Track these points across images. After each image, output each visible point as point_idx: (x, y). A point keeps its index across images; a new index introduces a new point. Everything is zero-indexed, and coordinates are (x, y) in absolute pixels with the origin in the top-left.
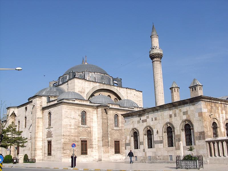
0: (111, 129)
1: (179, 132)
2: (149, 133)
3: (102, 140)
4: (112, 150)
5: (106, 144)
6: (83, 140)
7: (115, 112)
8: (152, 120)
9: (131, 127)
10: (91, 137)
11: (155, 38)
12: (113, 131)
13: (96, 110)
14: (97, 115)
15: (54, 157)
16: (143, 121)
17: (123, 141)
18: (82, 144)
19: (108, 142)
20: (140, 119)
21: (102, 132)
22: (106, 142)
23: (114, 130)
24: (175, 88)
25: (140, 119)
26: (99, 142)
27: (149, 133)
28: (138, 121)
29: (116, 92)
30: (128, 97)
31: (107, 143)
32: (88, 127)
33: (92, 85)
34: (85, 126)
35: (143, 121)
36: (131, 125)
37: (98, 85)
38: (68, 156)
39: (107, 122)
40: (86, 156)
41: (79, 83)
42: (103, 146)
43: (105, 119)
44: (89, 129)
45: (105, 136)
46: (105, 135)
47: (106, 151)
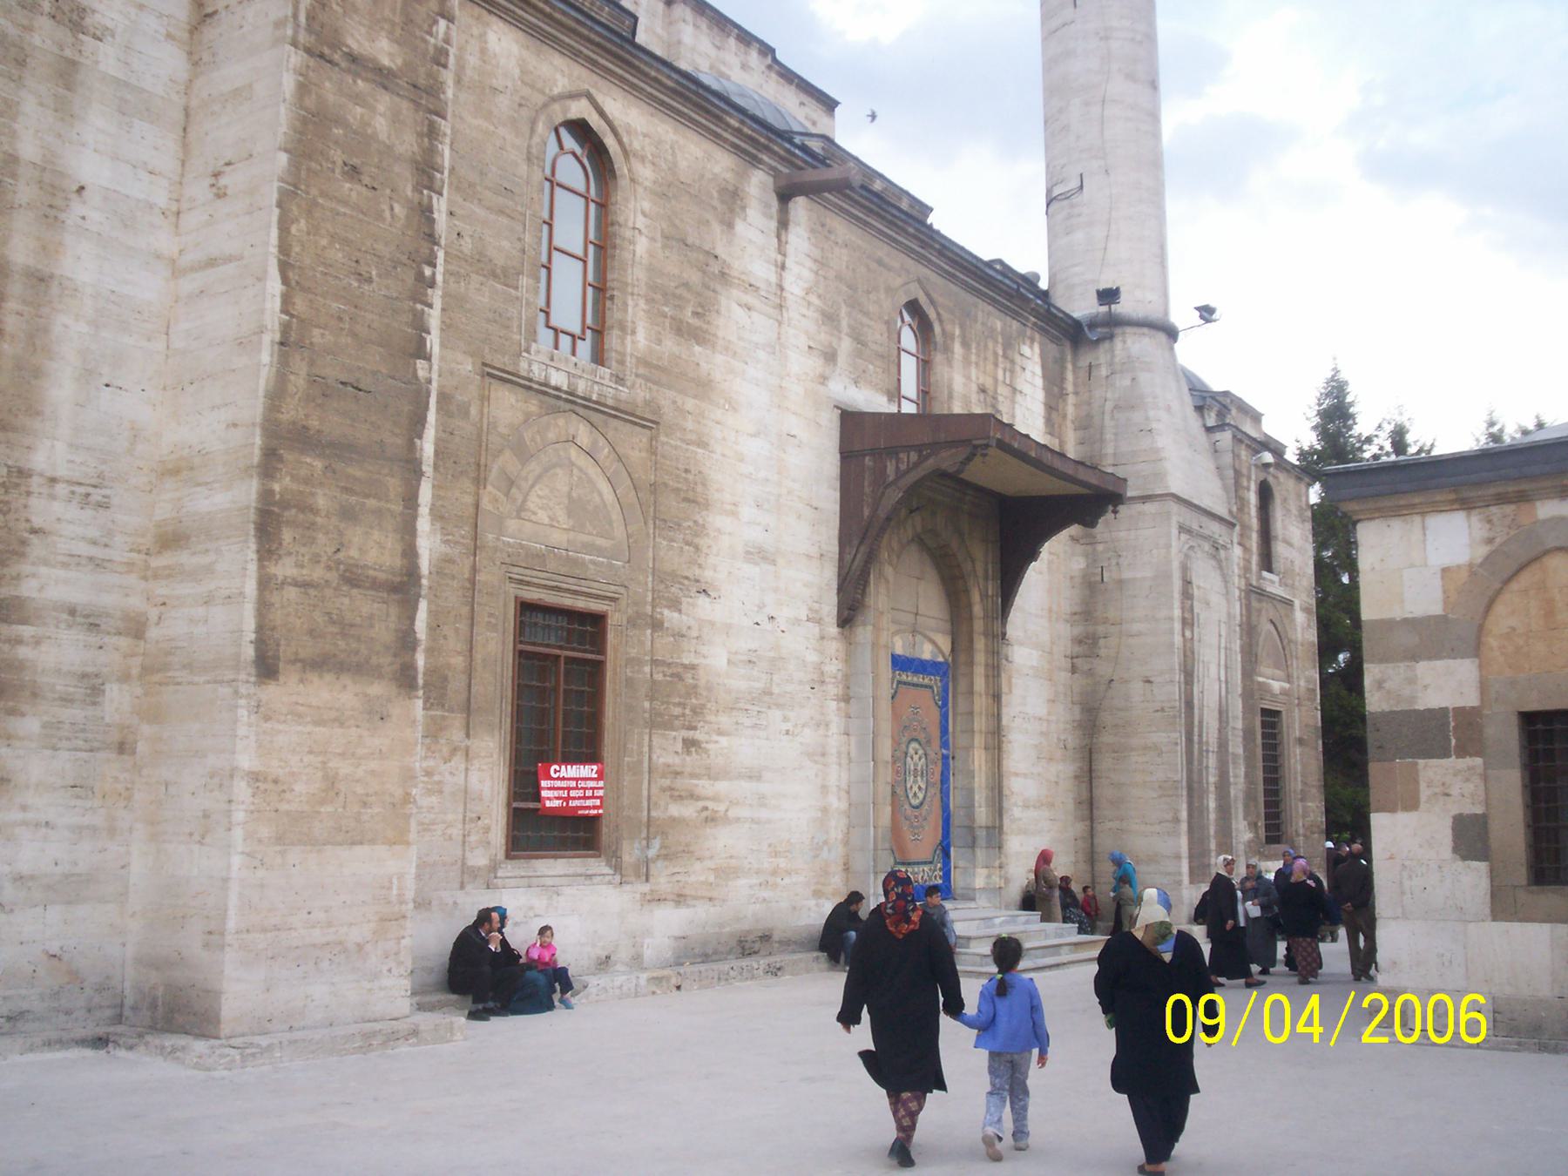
0: (467, 366)
4: (452, 773)
5: (345, 628)
7: (561, 85)
12: (507, 406)
17: (657, 625)
19: (404, 587)
22: (353, 578)
26: (184, 558)
31: (363, 605)
42: (266, 668)
43: (383, 77)
45: (338, 450)
46: (341, 421)
47: (331, 782)
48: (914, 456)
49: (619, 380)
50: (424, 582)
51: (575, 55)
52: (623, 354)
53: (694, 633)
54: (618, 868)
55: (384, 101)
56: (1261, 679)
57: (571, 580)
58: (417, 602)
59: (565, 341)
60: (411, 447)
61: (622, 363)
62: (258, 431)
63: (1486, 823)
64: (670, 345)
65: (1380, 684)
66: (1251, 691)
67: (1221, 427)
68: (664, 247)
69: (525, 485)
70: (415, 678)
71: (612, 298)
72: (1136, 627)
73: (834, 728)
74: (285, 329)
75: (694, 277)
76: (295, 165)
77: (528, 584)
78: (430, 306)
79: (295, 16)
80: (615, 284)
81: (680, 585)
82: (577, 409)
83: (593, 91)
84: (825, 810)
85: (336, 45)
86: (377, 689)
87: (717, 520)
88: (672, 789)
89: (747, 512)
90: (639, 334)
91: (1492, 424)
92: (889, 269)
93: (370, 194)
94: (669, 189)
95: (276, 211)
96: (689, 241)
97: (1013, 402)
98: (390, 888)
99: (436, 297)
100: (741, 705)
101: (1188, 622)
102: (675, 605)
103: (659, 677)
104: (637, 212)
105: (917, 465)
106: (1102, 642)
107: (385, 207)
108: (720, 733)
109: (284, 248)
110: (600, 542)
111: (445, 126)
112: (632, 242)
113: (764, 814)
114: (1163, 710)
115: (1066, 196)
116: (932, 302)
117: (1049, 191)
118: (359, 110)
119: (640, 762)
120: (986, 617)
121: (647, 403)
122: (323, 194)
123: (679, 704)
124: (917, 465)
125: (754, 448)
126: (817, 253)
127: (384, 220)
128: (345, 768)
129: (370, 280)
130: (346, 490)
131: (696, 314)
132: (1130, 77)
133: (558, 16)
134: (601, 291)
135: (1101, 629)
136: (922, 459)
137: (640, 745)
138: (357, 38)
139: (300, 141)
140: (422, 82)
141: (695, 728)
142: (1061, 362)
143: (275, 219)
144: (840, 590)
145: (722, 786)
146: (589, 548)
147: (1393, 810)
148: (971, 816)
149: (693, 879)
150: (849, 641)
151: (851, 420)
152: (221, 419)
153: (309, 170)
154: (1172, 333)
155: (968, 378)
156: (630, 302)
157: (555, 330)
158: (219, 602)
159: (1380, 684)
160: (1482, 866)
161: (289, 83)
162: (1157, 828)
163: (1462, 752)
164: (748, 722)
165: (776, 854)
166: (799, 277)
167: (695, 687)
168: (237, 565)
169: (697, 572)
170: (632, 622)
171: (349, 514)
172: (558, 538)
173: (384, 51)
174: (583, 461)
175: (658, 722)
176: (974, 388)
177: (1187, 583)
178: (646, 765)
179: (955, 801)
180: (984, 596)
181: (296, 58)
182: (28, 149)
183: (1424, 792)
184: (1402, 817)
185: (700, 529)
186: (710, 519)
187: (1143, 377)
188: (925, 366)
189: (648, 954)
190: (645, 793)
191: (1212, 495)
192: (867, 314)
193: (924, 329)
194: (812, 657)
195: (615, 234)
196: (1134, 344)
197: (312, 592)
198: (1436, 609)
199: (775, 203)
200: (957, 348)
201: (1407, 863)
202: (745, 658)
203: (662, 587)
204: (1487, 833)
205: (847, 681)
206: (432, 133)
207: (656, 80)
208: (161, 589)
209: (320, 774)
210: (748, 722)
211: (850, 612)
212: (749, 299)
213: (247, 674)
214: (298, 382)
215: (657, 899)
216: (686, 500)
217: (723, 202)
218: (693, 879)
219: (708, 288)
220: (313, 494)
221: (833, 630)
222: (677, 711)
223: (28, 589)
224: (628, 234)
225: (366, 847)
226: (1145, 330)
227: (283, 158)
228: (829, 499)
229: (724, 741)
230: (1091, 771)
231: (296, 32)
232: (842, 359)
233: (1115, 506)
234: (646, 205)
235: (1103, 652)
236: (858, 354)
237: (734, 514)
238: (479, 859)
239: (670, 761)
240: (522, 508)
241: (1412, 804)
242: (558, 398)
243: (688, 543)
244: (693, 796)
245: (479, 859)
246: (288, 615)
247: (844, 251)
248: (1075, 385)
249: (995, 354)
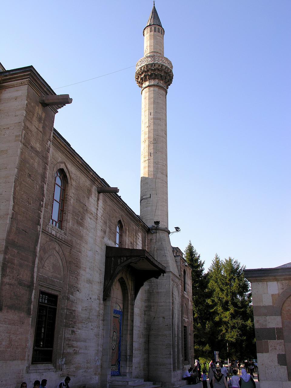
7: (60, 160)
17: (68, 299)
21: (10, 211)
22: (20, 283)
47: (11, 341)
48: (125, 259)
49: (65, 234)
50: (35, 285)
52: (67, 228)
53: (75, 302)
54: (55, 367)
55: (37, 159)
56: (184, 318)
57: (52, 286)
58: (33, 291)
59: (54, 223)
61: (66, 230)
62: (5, 241)
63: (285, 356)
64: (76, 226)
65: (258, 322)
66: (183, 321)
67: (178, 256)
68: (76, 202)
69: (45, 260)
70: (30, 312)
71: (65, 213)
72: (163, 304)
73: (101, 328)
74: (13, 214)
75: (81, 210)
76: (18, 172)
77: (43, 286)
78: (42, 212)
79: (22, 135)
80: (66, 210)
81: (74, 288)
82: (56, 240)
83: (66, 162)
84: (98, 351)
85: (29, 144)
86: (22, 315)
87: (82, 272)
88: (68, 344)
89: (88, 270)
90: (70, 224)
91: (217, 258)
92: (116, 212)
93: (32, 182)
94: (78, 188)
95: (14, 183)
96: (81, 201)
98: (20, 374)
99: (43, 209)
100: (83, 321)
101: (173, 304)
103: (68, 313)
104: (71, 192)
105: (126, 261)
106: (152, 308)
107: (35, 186)
108: (79, 329)
109: (14, 193)
110: (58, 276)
112: (70, 200)
114: (167, 325)
115: (146, 198)
116: (123, 221)
117: (141, 197)
118: (32, 160)
119: (62, 336)
120: (131, 300)
121: (71, 241)
122: (23, 181)
123: (71, 320)
124: (126, 261)
125: (90, 254)
126: (104, 207)
127: (34, 189)
129: (30, 204)
130: (21, 259)
131: (81, 219)
132: (162, 173)
133: (61, 143)
134: (62, 211)
135: (152, 304)
136: (127, 259)
137: (63, 332)
138: (33, 143)
139: (20, 166)
140: (44, 155)
141: (74, 327)
142: (145, 237)
143: (13, 185)
144: (104, 292)
145: (79, 343)
146: (56, 278)
147: (263, 353)
148: (126, 353)
149: (71, 370)
150: (105, 305)
151: (109, 249)
153: (21, 174)
154: (169, 233)
155: (129, 240)
156: (69, 215)
157: (53, 220)
159: (258, 322)
160: (286, 367)
161: (19, 151)
162: (165, 356)
163: (279, 338)
164: (84, 326)
166: (100, 212)
167: (75, 316)
169: (77, 285)
172: (50, 274)
173: (38, 146)
175: (67, 326)
176: (130, 242)
177: (173, 293)
178: (63, 337)
179: (123, 348)
181: (21, 145)
183: (270, 349)
184: (265, 354)
185: (78, 274)
186: (80, 271)
187: (163, 243)
188: (121, 236)
190: (63, 346)
191: (177, 274)
192: (112, 222)
193: (121, 227)
194: (98, 309)
195: (67, 198)
196: (161, 234)
197: (12, 287)
198: (271, 304)
199: (97, 194)
201: (266, 366)
202: (85, 308)
203: (70, 289)
204: (286, 358)
205: (105, 315)
207: (78, 161)
209: (8, 339)
210: (84, 326)
212: (91, 216)
214: (14, 229)
216: (76, 266)
217: (88, 192)
218: (71, 370)
219: (84, 213)
220: (14, 259)
221: (102, 302)
222: (71, 322)
224: (70, 198)
225: (16, 361)
226: (164, 232)
227: (16, 170)
229: (79, 331)
230: (149, 341)
231: (22, 139)
232: (107, 233)
233: (163, 274)
234: (74, 191)
235: (153, 310)
236: (110, 232)
237: (85, 270)
239: (68, 336)
240: (43, 266)
241: (267, 351)
242: (53, 237)
243: (76, 278)
244: (73, 347)
246: (6, 293)
247: (109, 207)
248: (148, 243)
249: (134, 234)
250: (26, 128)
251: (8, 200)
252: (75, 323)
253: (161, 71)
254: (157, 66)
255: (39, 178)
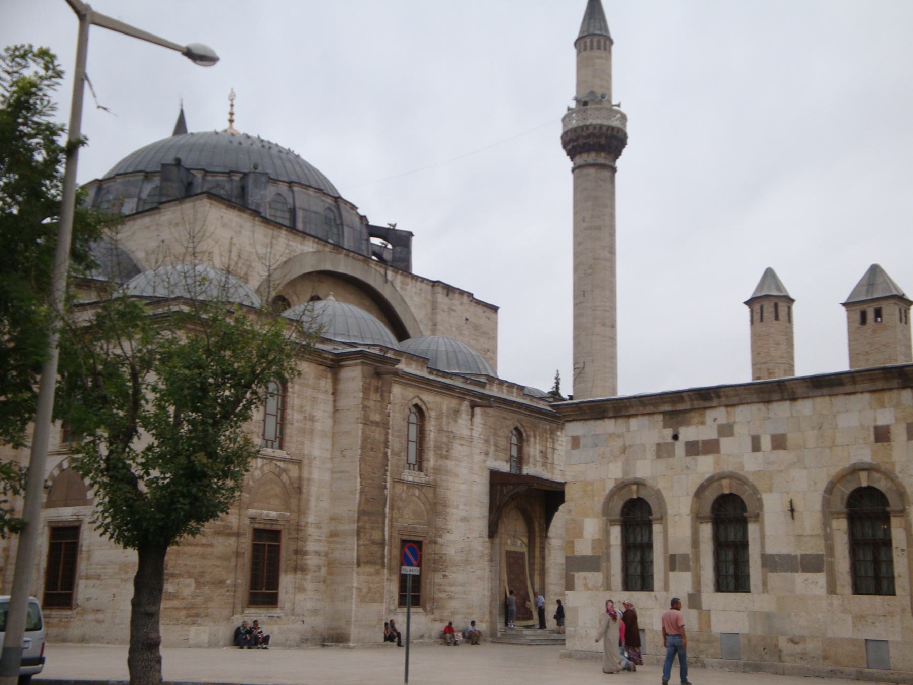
1: (679, 528)
2: (729, 513)
3: (358, 535)
6: (262, 526)
7: (411, 395)
8: (756, 446)
9: (615, 472)
10: (301, 511)
11: (599, 48)
13: (329, 375)
14: (335, 401)
15: (91, 617)
16: (693, 449)
17: (435, 543)
18: (256, 549)
19: (382, 544)
20: (675, 437)
21: (358, 487)
22: (373, 543)
23: (403, 482)
24: (775, 300)
25: (675, 437)
26: (338, 539)
27: (729, 513)
28: (659, 445)
29: (386, 292)
30: (439, 327)
31: (375, 548)
32: (292, 461)
33: (285, 246)
34: (280, 453)
35: (693, 449)
36: (611, 466)
37: (311, 250)
38: (184, 613)
39: (382, 439)
40: (276, 612)
41: (224, 225)
42: (358, 565)
43: (377, 424)
44: (294, 471)
46: (372, 508)
47: (369, 588)
51: (414, 386)
60: (384, 511)
81: (439, 531)
86: (378, 567)
87: (451, 511)
89: (461, 507)
90: (431, 460)
97: (553, 453)
99: (388, 474)
102: (441, 537)
111: (390, 431)
113: (464, 596)
116: (523, 426)
128: (372, 586)
132: (603, 325)
145: (453, 588)
150: (492, 543)
152: (350, 507)
158: (350, 549)
165: (190, 393)
168: (353, 542)
170: (429, 543)
171: (372, 528)
172: (411, 522)
174: (417, 500)
175: (435, 570)
180: (540, 524)
181: (361, 426)
182: (306, 452)
189: (433, 635)
194: (480, 548)
200: (532, 440)
206: (387, 434)
208: (332, 546)
211: (493, 531)
212: (461, 442)
213: (355, 566)
215: (435, 620)
221: (487, 540)
223: (308, 548)
228: (486, 499)
236: (496, 450)
238: (392, 608)
244: (445, 591)
245: (392, 608)
250: (365, 408)
251: (356, 478)
252: (446, 567)
253: (600, 137)
254: (591, 130)
255: (382, 446)
